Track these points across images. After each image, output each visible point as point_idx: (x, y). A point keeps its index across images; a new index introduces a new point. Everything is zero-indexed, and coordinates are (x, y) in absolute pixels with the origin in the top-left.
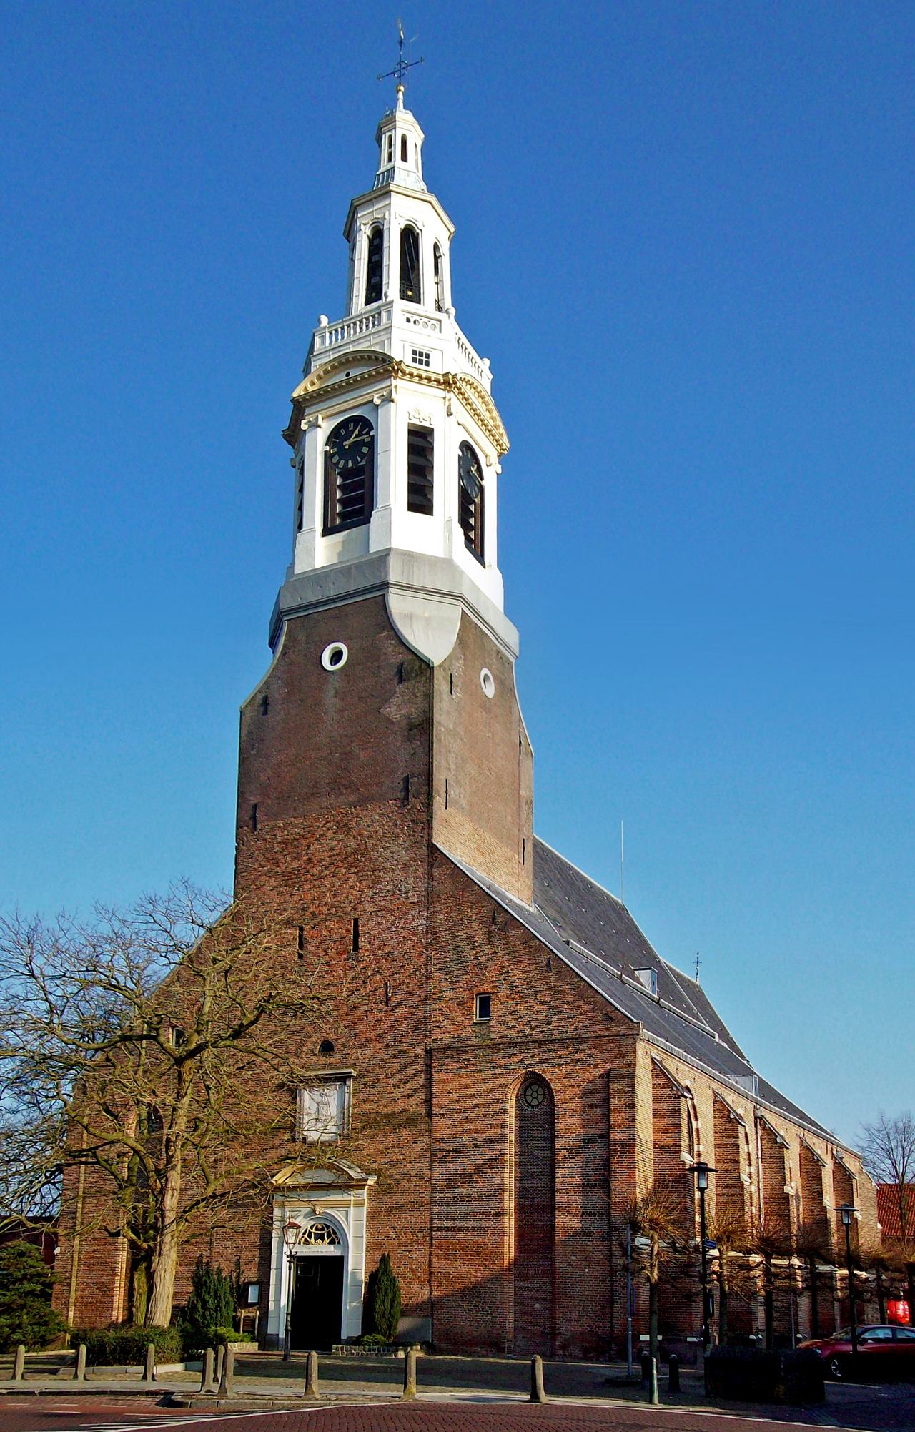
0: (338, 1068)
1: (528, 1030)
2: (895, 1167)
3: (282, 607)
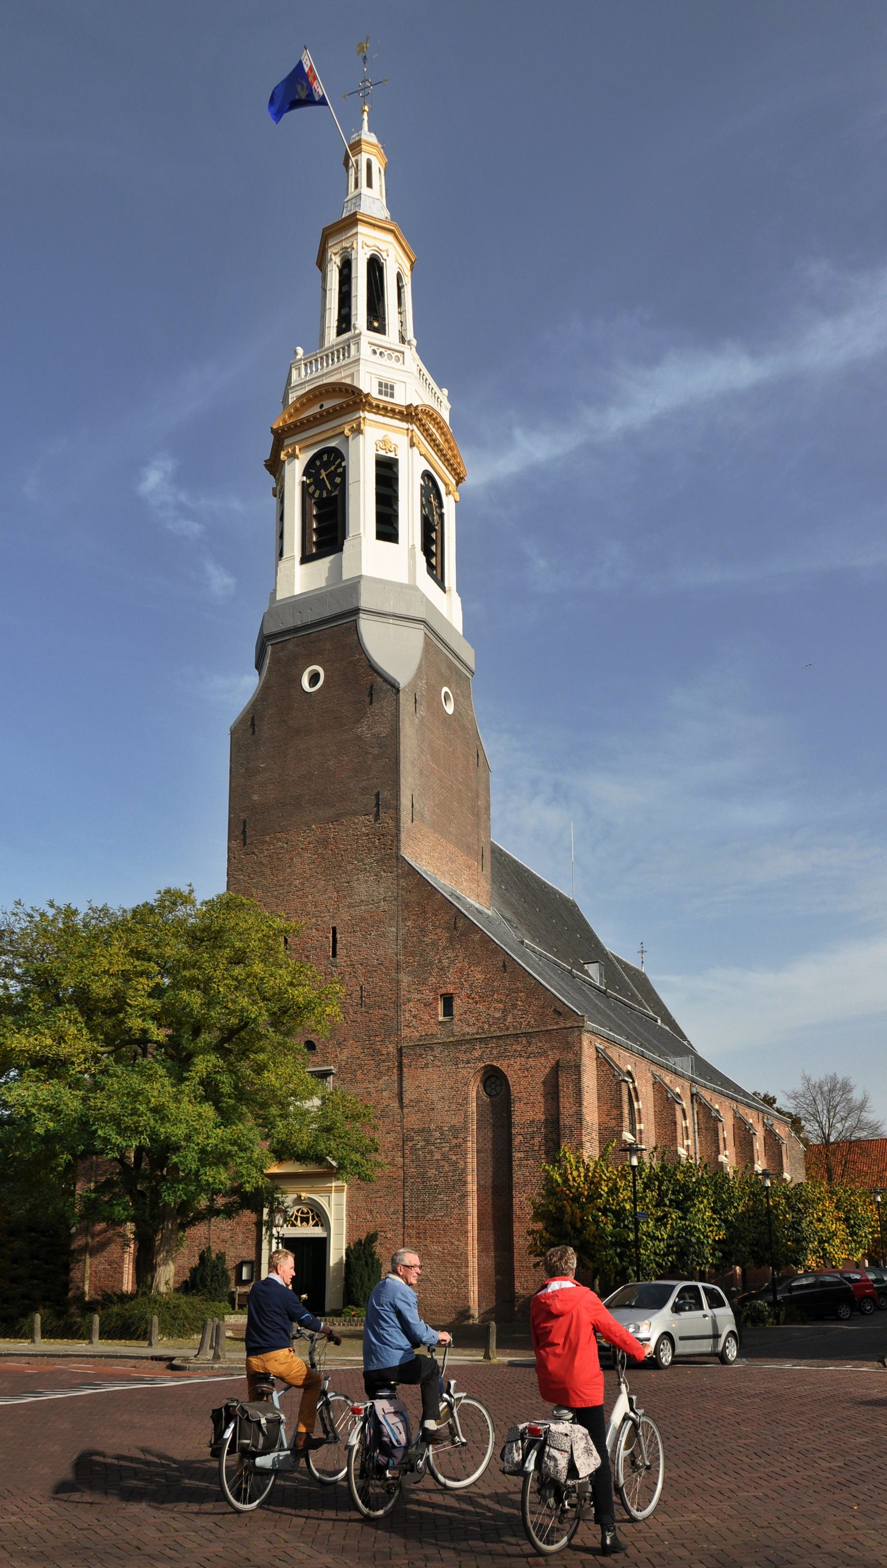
0: (320, 1066)
1: (486, 1026)
2: (822, 1128)
3: (265, 632)
